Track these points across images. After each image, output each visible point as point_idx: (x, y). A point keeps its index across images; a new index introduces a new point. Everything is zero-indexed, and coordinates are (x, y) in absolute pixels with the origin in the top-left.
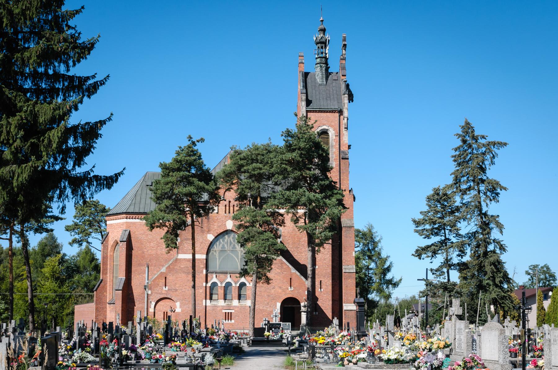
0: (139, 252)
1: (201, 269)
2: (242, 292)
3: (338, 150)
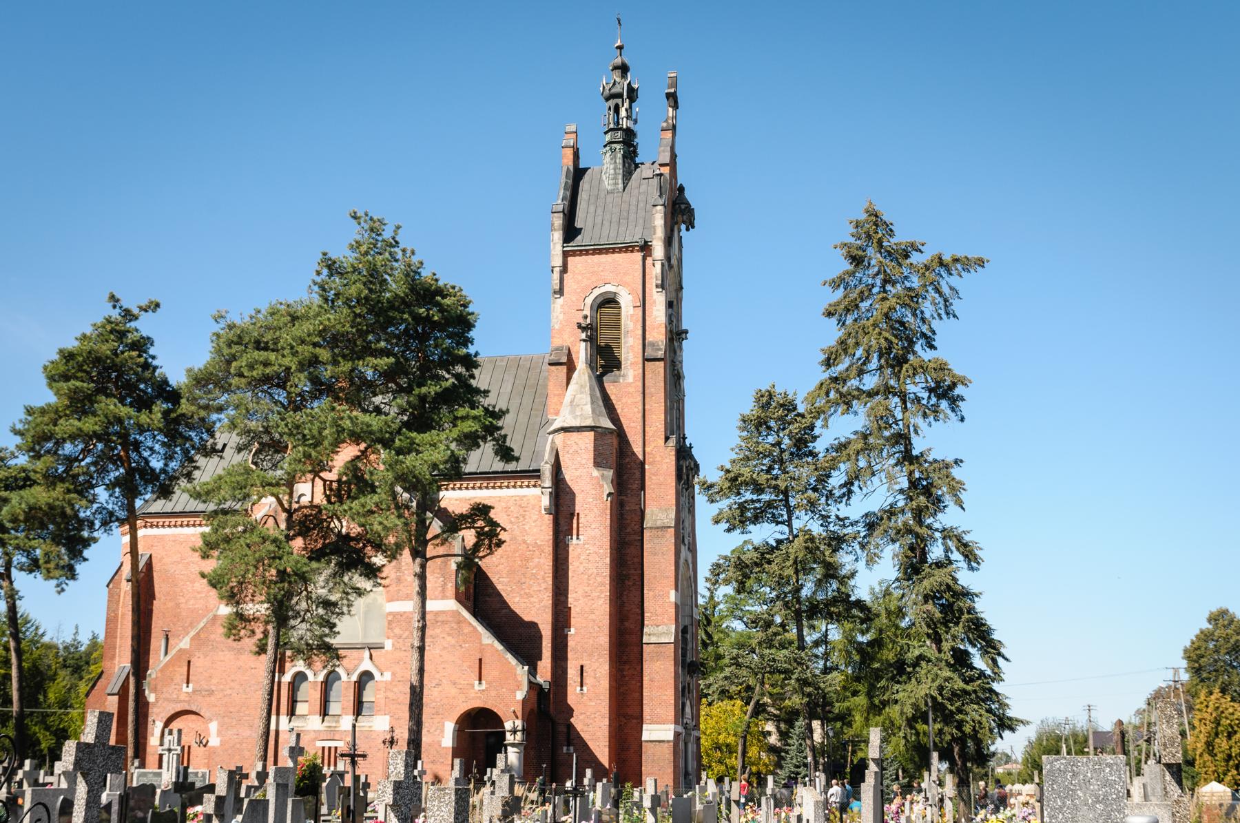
2: (367, 696)
3: (641, 342)
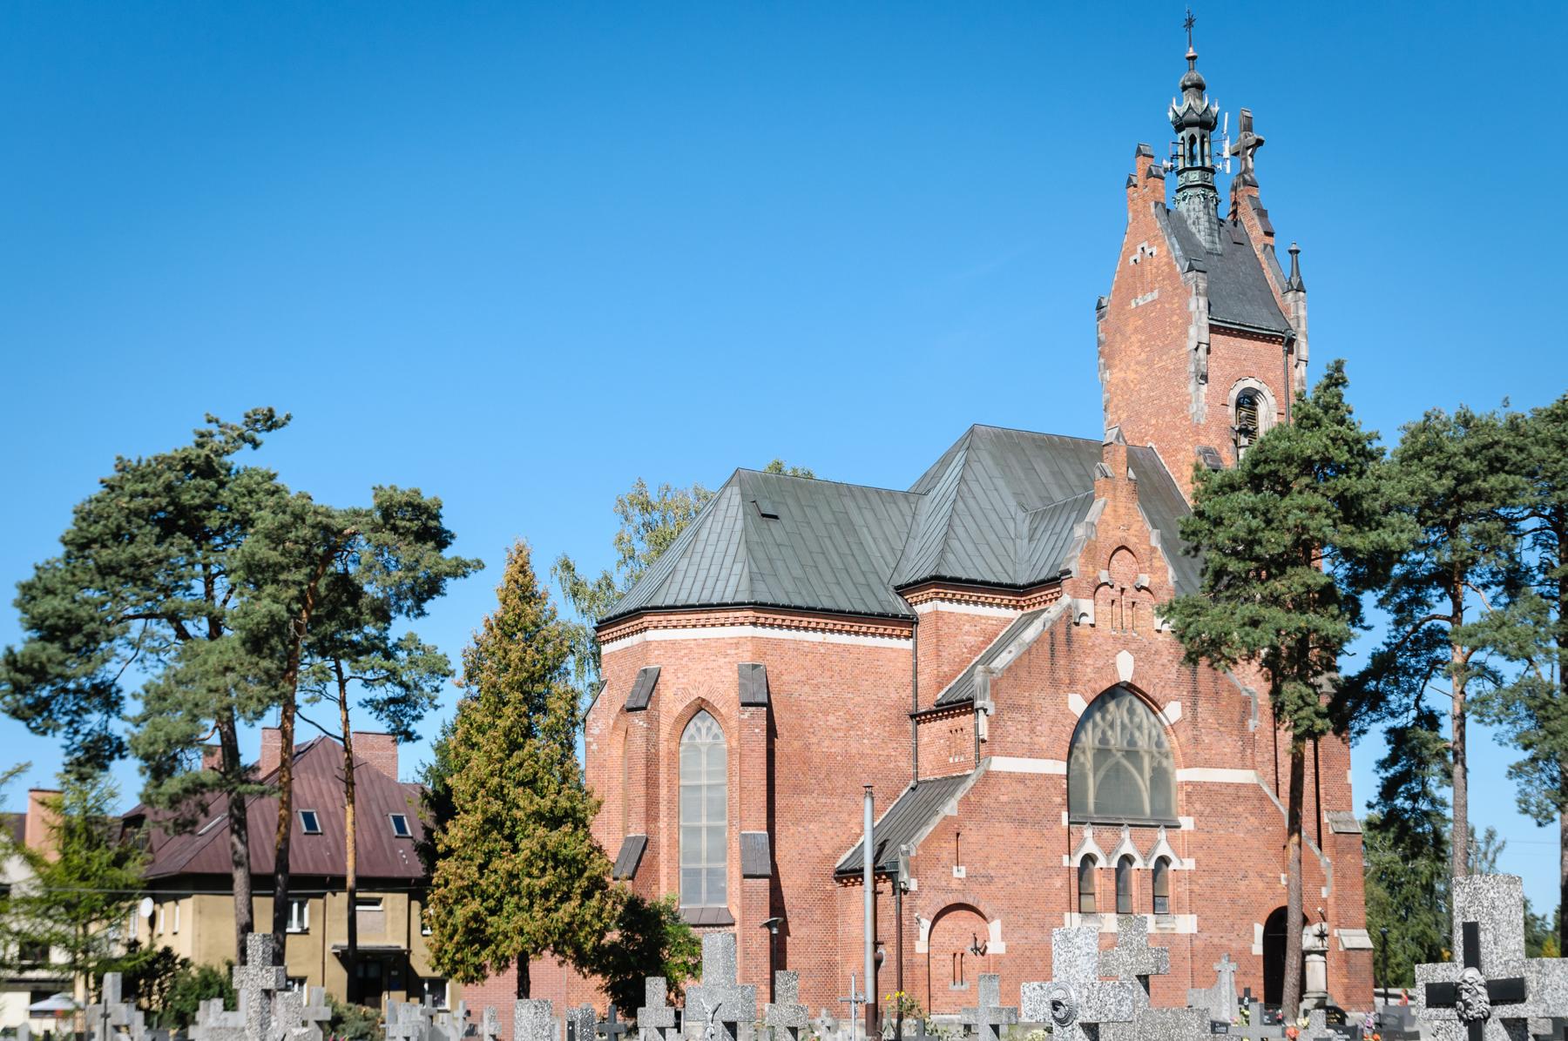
0: (797, 744)
1: (1056, 810)
